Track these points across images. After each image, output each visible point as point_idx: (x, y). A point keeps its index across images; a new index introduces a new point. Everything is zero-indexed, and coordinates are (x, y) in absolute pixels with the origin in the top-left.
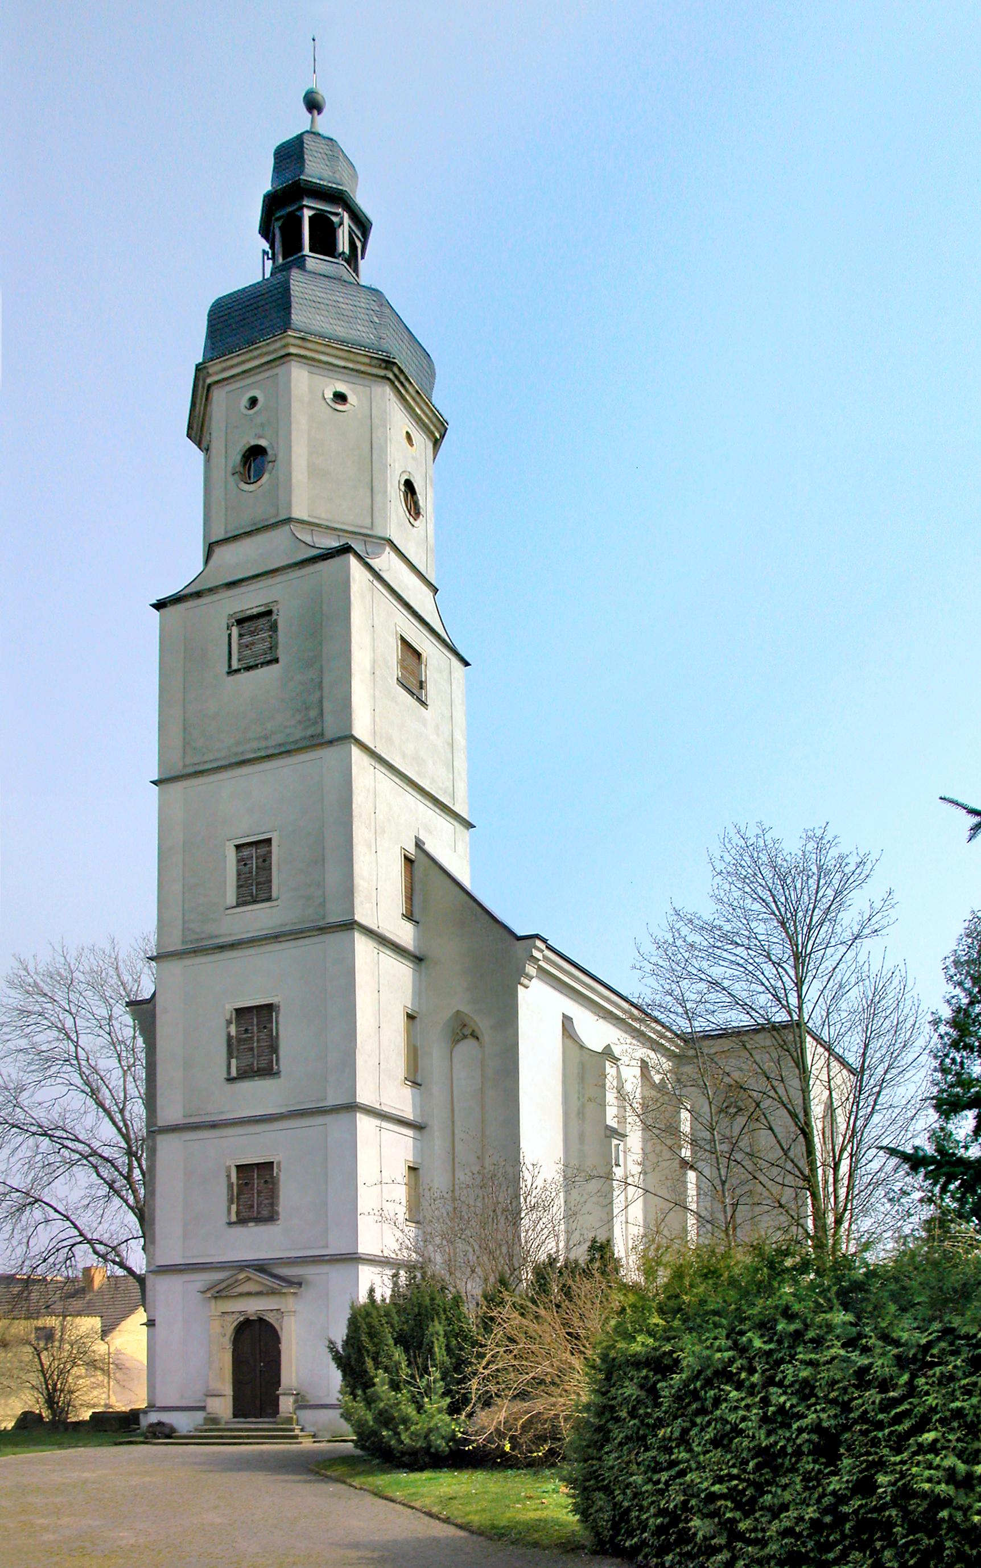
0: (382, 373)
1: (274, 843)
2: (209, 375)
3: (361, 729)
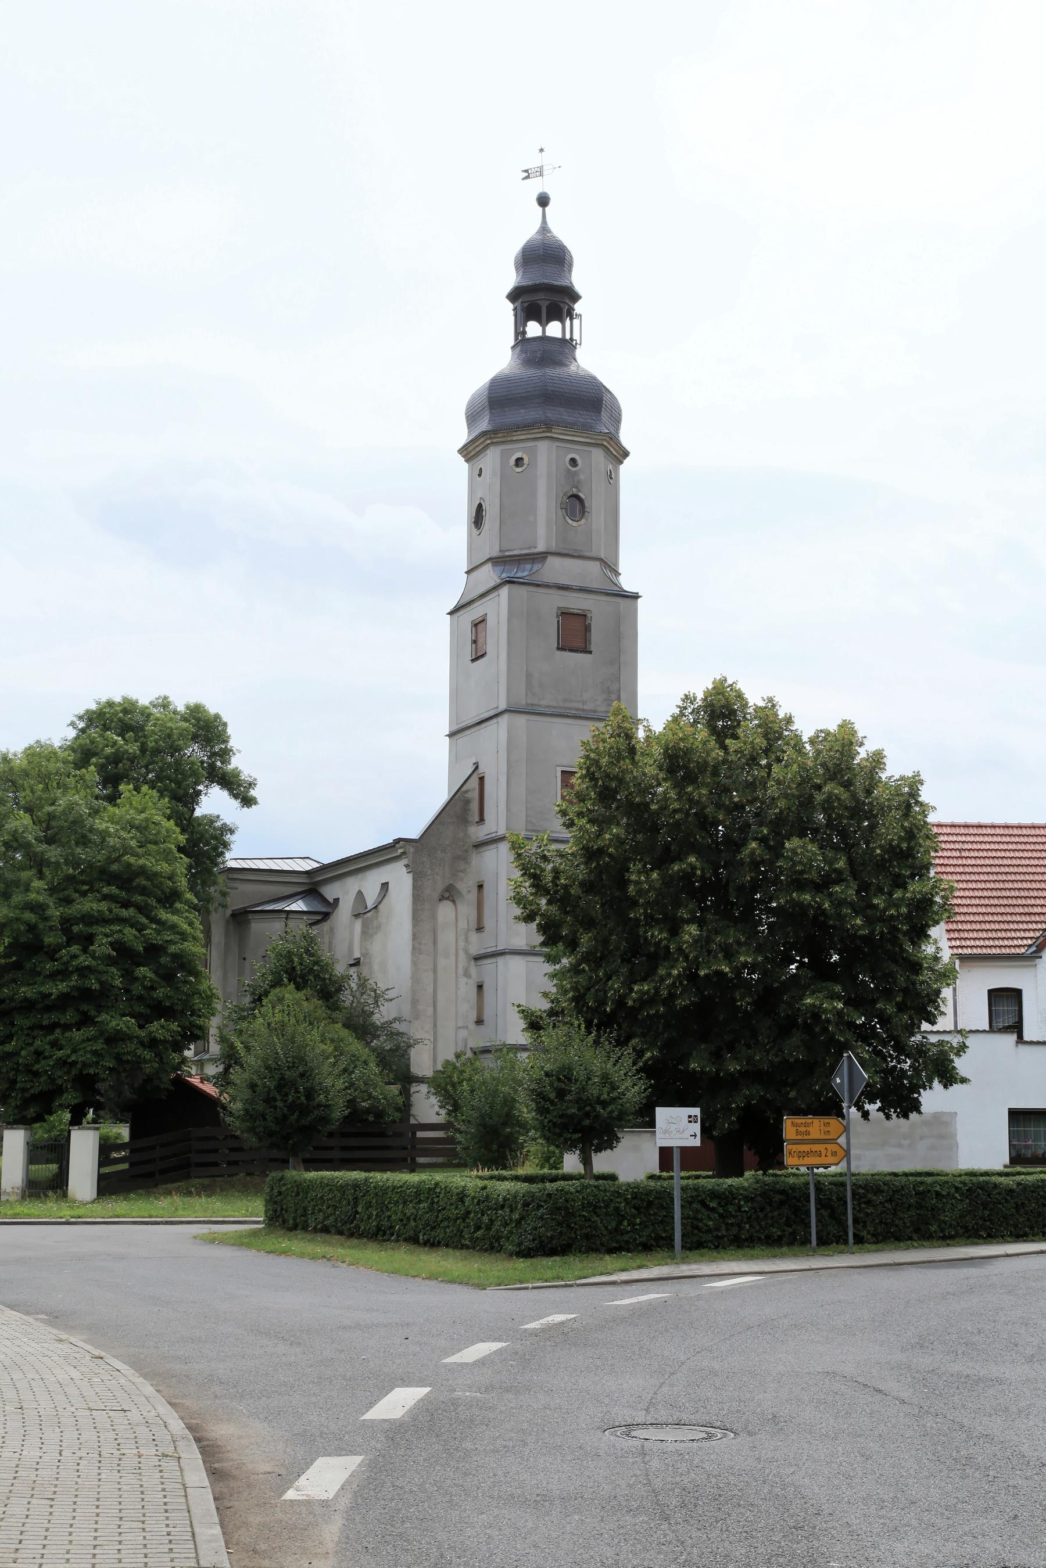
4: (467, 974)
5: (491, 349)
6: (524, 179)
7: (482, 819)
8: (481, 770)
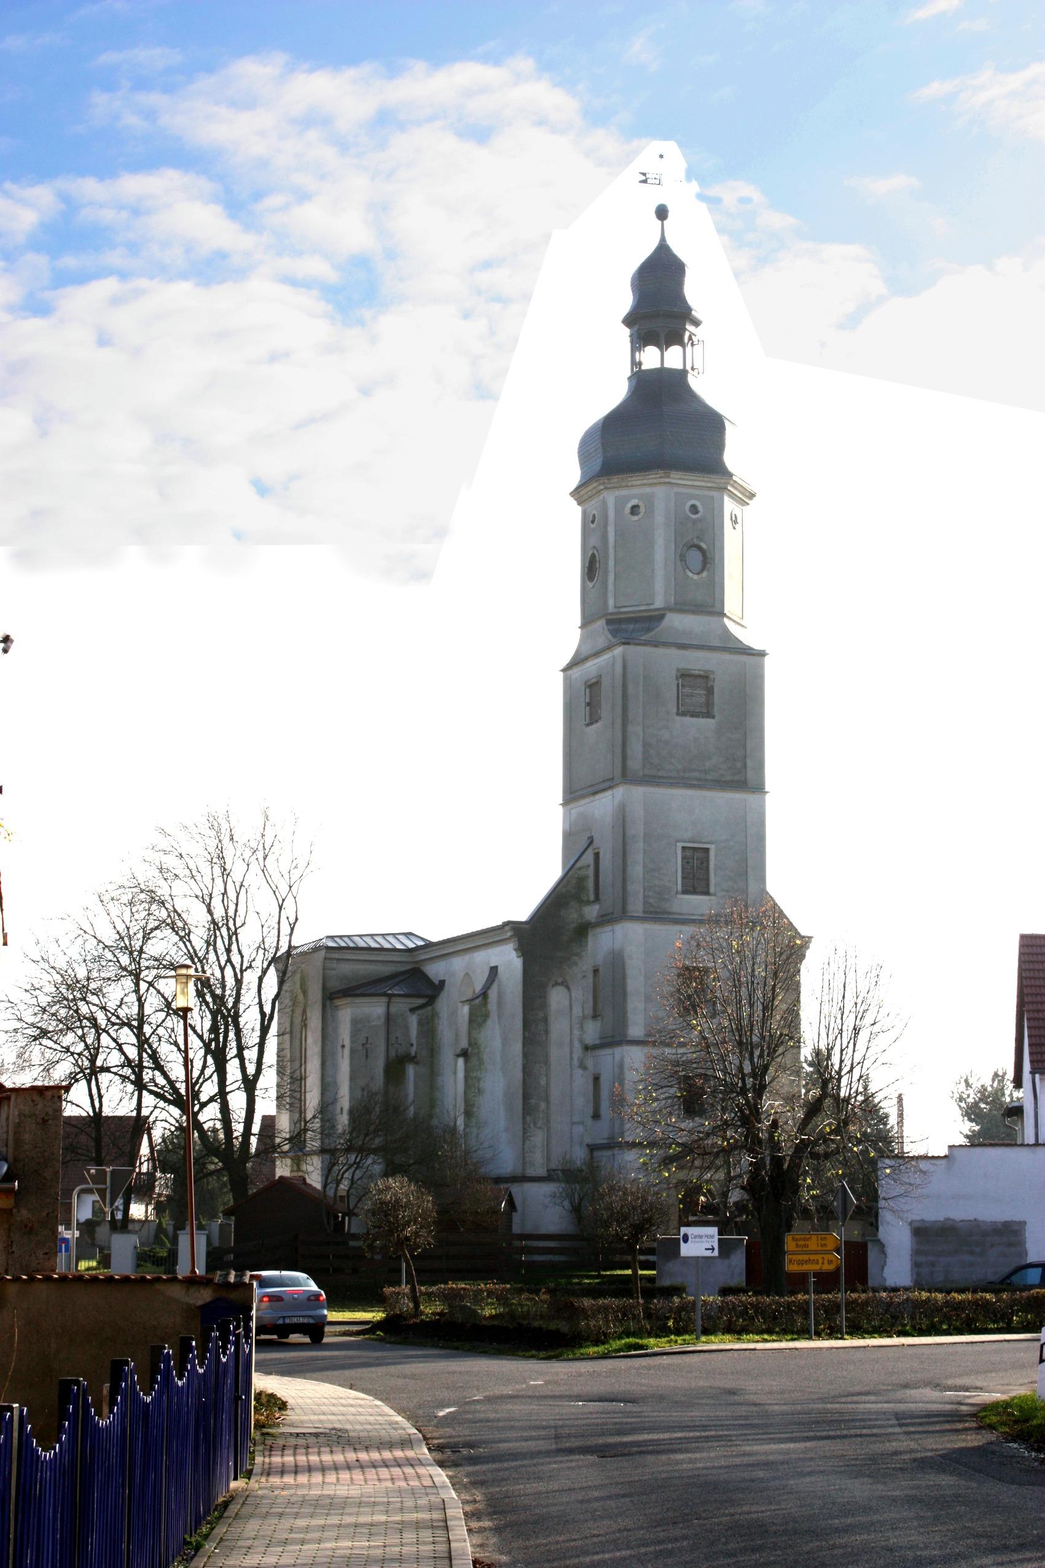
1: (712, 854)
4: (583, 1066)
5: (601, 375)
6: (641, 182)
7: (597, 899)
8: (596, 844)
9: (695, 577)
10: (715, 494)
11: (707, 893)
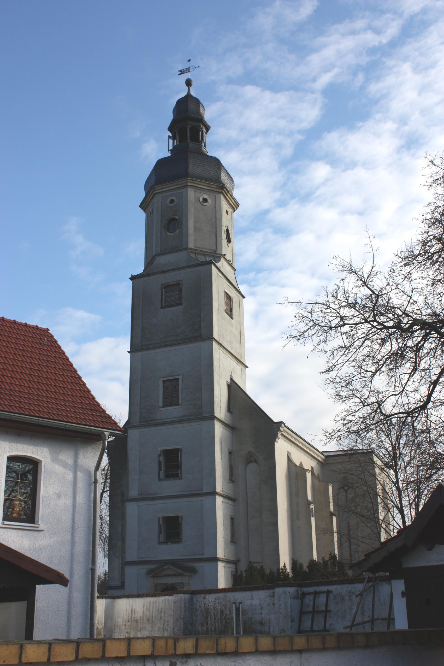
0: (220, 191)
1: (180, 381)
2: (155, 190)
3: (215, 335)
9: (172, 234)
10: (184, 190)
11: (178, 404)
